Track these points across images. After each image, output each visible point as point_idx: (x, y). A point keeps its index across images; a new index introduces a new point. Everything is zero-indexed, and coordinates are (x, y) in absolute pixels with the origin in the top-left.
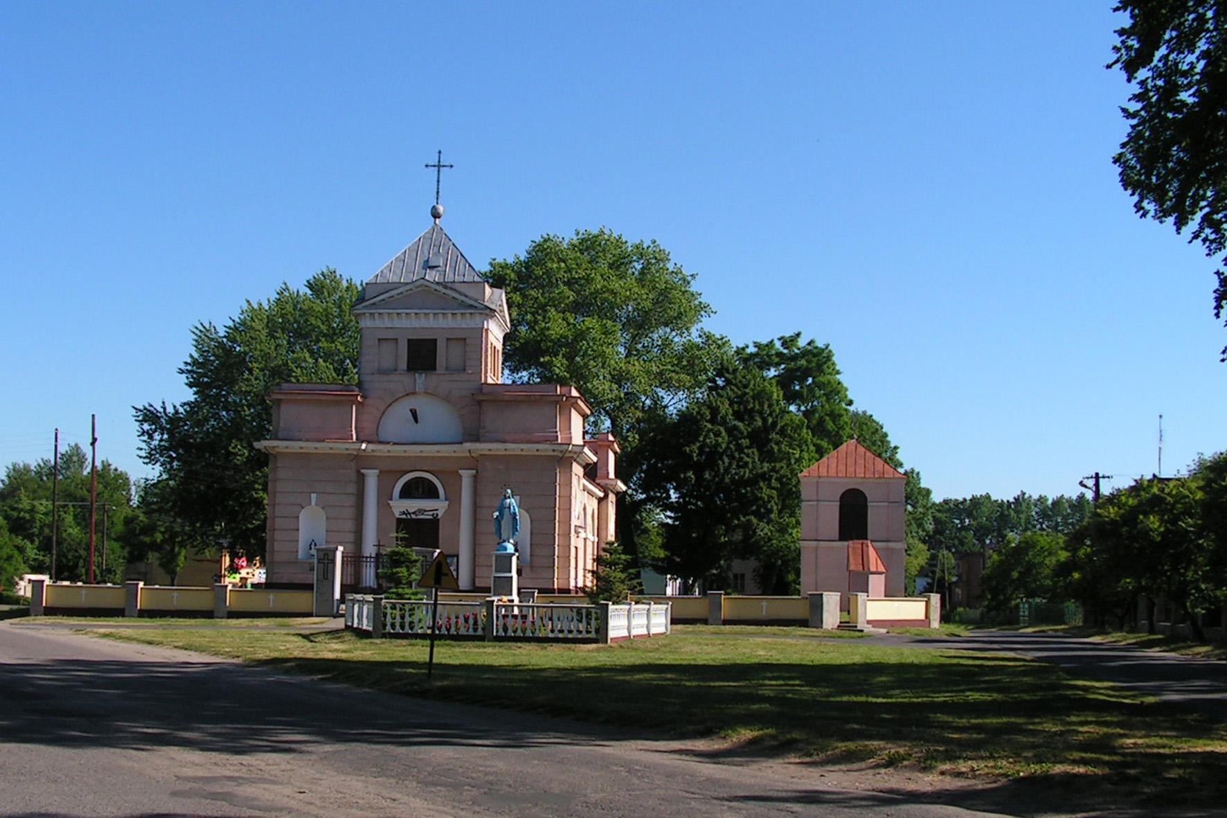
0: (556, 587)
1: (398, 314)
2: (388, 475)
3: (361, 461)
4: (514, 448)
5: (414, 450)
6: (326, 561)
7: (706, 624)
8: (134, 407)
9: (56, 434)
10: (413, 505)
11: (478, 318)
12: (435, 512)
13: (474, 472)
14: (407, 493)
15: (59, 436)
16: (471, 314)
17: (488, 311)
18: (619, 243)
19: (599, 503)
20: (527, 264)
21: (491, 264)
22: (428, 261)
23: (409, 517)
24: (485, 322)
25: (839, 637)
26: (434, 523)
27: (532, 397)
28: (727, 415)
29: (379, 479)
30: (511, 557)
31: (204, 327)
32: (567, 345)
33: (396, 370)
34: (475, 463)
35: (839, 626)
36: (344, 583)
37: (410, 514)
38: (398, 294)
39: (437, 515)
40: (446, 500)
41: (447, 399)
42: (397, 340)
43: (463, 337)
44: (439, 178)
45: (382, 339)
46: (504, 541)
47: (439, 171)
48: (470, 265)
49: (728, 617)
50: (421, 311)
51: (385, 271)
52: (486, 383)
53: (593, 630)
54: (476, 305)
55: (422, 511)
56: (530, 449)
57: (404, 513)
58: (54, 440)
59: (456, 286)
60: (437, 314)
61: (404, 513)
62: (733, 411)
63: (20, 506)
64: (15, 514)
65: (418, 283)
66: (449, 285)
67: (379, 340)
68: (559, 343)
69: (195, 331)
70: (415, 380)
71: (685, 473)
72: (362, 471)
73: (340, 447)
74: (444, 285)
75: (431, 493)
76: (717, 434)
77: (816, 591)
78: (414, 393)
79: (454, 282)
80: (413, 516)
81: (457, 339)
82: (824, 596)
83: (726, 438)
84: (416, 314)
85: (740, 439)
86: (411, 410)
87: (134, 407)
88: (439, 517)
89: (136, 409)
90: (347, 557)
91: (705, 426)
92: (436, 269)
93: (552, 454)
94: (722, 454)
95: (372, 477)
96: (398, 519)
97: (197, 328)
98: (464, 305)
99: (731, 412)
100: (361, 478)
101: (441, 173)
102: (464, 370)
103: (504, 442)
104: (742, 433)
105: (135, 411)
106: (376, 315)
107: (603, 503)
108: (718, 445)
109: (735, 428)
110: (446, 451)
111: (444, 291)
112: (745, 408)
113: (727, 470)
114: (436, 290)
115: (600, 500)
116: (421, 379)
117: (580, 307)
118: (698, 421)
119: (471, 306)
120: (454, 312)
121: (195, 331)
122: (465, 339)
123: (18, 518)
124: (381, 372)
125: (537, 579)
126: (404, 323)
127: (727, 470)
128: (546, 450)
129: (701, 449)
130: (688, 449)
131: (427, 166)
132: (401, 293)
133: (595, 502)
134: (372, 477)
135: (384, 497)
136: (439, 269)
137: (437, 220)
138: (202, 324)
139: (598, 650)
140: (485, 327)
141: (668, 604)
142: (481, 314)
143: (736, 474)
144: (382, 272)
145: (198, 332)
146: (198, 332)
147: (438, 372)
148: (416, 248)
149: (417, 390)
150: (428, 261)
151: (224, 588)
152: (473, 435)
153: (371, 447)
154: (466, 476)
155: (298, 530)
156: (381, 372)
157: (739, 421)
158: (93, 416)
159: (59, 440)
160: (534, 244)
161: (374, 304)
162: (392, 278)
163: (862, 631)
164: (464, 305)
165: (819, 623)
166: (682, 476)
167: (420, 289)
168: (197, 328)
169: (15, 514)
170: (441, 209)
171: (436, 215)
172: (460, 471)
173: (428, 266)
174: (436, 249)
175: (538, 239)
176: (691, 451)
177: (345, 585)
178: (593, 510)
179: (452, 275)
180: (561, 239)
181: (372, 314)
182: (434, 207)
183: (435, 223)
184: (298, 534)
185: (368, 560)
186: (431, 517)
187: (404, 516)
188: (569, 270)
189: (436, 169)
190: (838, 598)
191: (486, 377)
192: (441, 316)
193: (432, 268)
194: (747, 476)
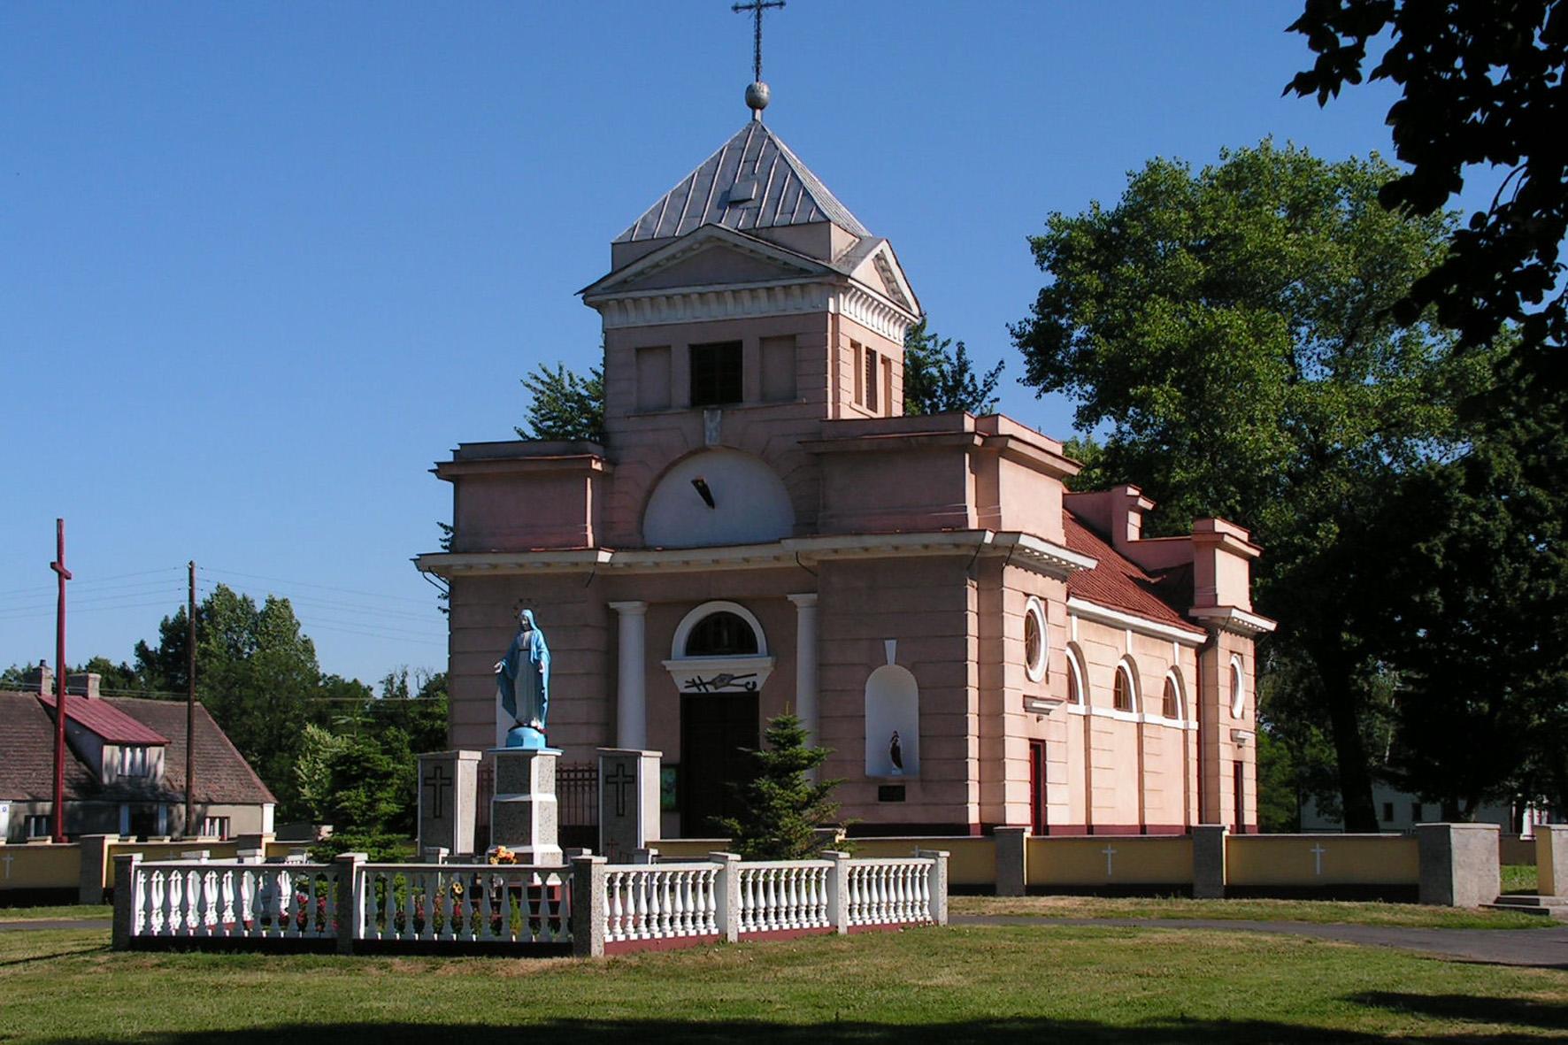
0: (974, 817)
1: (668, 298)
2: (662, 612)
3: (608, 584)
4: (880, 546)
5: (702, 560)
6: (620, 779)
7: (1191, 897)
8: (441, 525)
9: (191, 571)
10: (710, 667)
11: (815, 293)
12: (751, 679)
13: (814, 596)
14: (702, 643)
15: (195, 575)
16: (802, 286)
17: (832, 279)
18: (1302, 167)
19: (1198, 655)
20: (1117, 220)
21: (1049, 223)
22: (729, 192)
23: (703, 690)
24: (831, 301)
25: (1522, 927)
26: (750, 699)
27: (912, 440)
28: (1509, 475)
29: (646, 618)
30: (531, 758)
31: (550, 376)
32: (1182, 362)
33: (669, 407)
34: (814, 577)
35: (1498, 900)
36: (565, 823)
37: (704, 685)
38: (668, 259)
39: (754, 684)
40: (769, 655)
41: (765, 456)
42: (669, 347)
43: (787, 332)
44: (758, 30)
45: (651, 349)
46: (520, 725)
47: (759, 16)
48: (806, 193)
49: (1238, 880)
50: (711, 288)
51: (649, 220)
52: (837, 421)
53: (564, 924)
54: (810, 267)
55: (725, 679)
56: (913, 544)
57: (694, 684)
58: (187, 582)
59: (778, 235)
60: (739, 291)
61: (694, 684)
62: (1524, 467)
63: (437, 710)
64: (427, 723)
65: (701, 235)
66: (764, 233)
67: (638, 350)
68: (1165, 358)
69: (533, 383)
70: (703, 426)
71: (1423, 591)
72: (613, 605)
73: (562, 561)
74: (752, 233)
75: (743, 642)
76: (1490, 513)
77: (422, 819)
78: (703, 450)
79: (772, 226)
80: (711, 689)
81: (780, 338)
82: (1452, 831)
83: (1509, 521)
84: (700, 294)
85: (1541, 521)
86: (695, 483)
87: (441, 525)
88: (758, 689)
89: (445, 527)
90: (483, 771)
91: (1457, 500)
92: (741, 206)
93: (954, 552)
94: (1497, 553)
95: (632, 621)
96: (683, 695)
97: (536, 378)
98: (788, 270)
99: (1519, 469)
100: (613, 619)
101: (763, 19)
102: (795, 397)
103: (859, 533)
104: (1542, 509)
105: (443, 530)
106: (629, 304)
107: (1208, 655)
108: (1488, 534)
109: (1530, 500)
110: (760, 557)
111: (751, 245)
112: (1552, 460)
113: (1512, 582)
114: (736, 245)
115: (1201, 650)
116: (713, 421)
117: (1218, 289)
118: (1442, 490)
119: (802, 272)
120: (768, 285)
121: (533, 383)
122: (793, 337)
123: (432, 730)
124: (643, 412)
125: (936, 804)
126: (681, 315)
127: (1512, 582)
128: (939, 543)
129: (1451, 545)
130: (1423, 547)
131: (736, 8)
132: (674, 257)
133: (1190, 654)
134: (632, 621)
135: (657, 650)
136: (749, 204)
137: (758, 112)
138: (545, 371)
139: (563, 972)
140: (832, 309)
141: (936, 856)
142: (820, 284)
143: (1530, 590)
144: (644, 220)
145: (540, 387)
146: (540, 387)
147: (746, 405)
148: (709, 171)
149: (707, 442)
150: (729, 192)
151: (258, 839)
152: (808, 524)
153: (624, 557)
154: (803, 603)
155: (495, 723)
156: (643, 412)
157: (1537, 485)
158: (59, 521)
159: (196, 584)
160: (1132, 179)
161: (625, 282)
162: (659, 229)
163: (1546, 912)
164: (788, 270)
165: (1443, 893)
166: (1417, 599)
167: (705, 247)
168: (536, 378)
169: (427, 723)
170: (764, 91)
171: (754, 103)
172: (790, 597)
173: (730, 202)
174: (749, 168)
175: (1140, 168)
176: (1430, 550)
177: (565, 827)
178: (1068, 658)
179: (770, 213)
180: (1184, 167)
181: (620, 302)
182: (750, 86)
183: (754, 119)
184: (495, 730)
185: (580, 775)
186: (743, 689)
187: (694, 690)
188: (1198, 221)
189: (754, 11)
190: (1496, 835)
191: (837, 409)
192: (746, 296)
193: (735, 204)
194: (1552, 593)
